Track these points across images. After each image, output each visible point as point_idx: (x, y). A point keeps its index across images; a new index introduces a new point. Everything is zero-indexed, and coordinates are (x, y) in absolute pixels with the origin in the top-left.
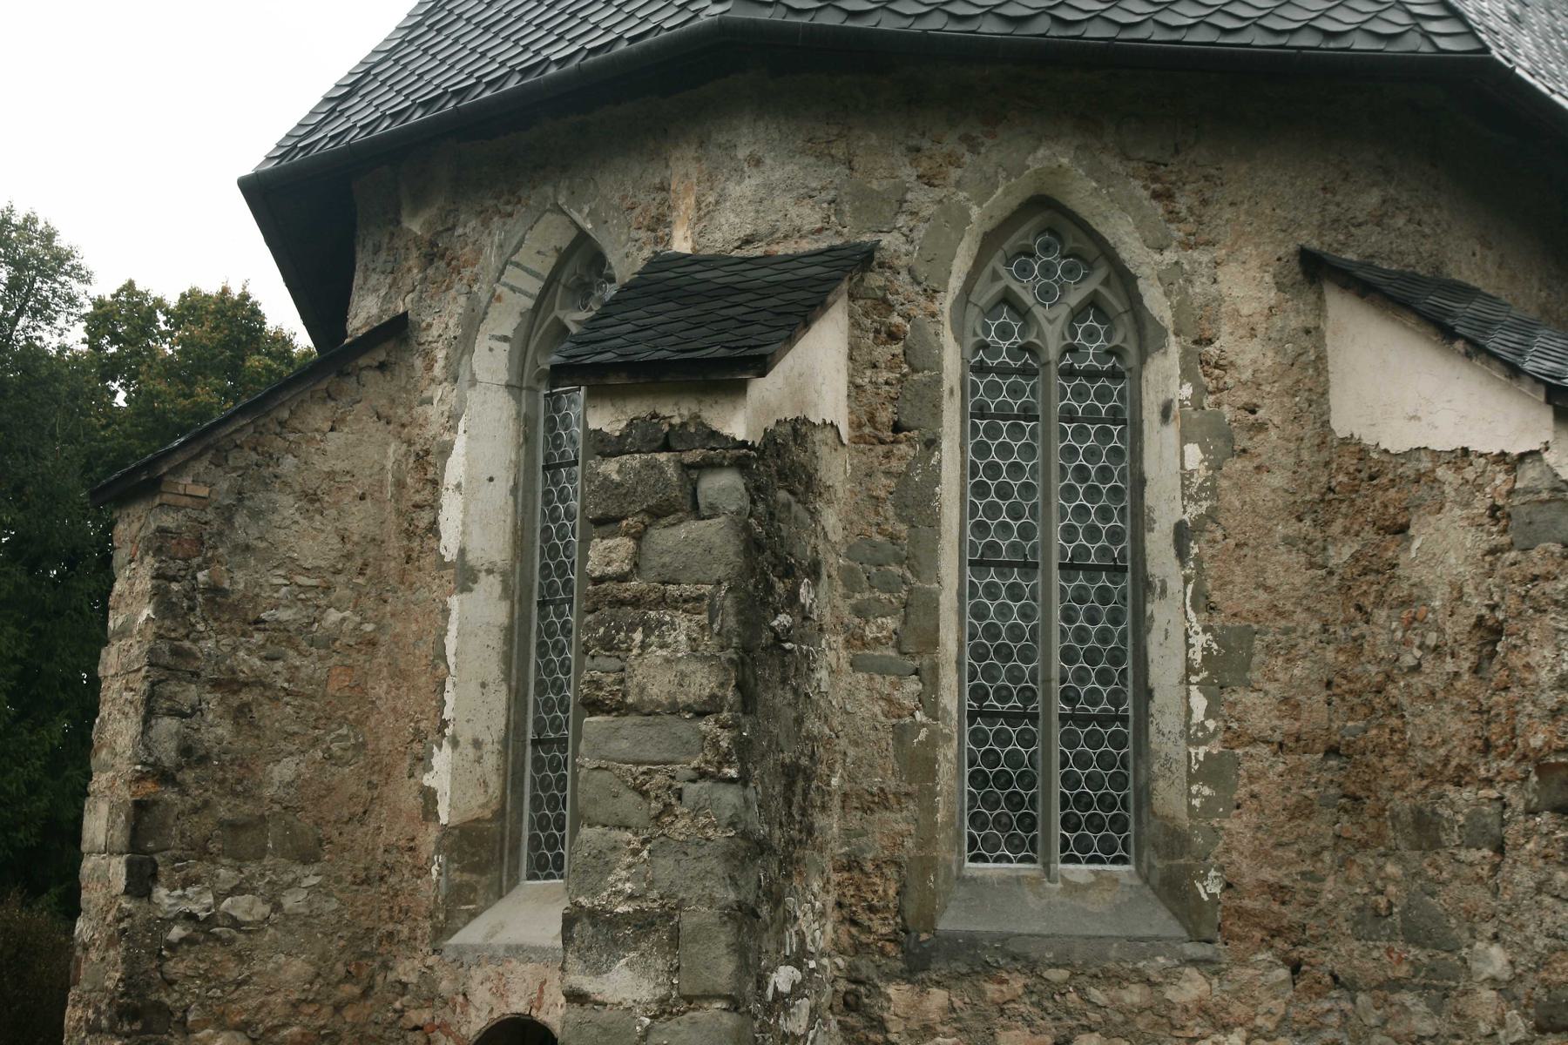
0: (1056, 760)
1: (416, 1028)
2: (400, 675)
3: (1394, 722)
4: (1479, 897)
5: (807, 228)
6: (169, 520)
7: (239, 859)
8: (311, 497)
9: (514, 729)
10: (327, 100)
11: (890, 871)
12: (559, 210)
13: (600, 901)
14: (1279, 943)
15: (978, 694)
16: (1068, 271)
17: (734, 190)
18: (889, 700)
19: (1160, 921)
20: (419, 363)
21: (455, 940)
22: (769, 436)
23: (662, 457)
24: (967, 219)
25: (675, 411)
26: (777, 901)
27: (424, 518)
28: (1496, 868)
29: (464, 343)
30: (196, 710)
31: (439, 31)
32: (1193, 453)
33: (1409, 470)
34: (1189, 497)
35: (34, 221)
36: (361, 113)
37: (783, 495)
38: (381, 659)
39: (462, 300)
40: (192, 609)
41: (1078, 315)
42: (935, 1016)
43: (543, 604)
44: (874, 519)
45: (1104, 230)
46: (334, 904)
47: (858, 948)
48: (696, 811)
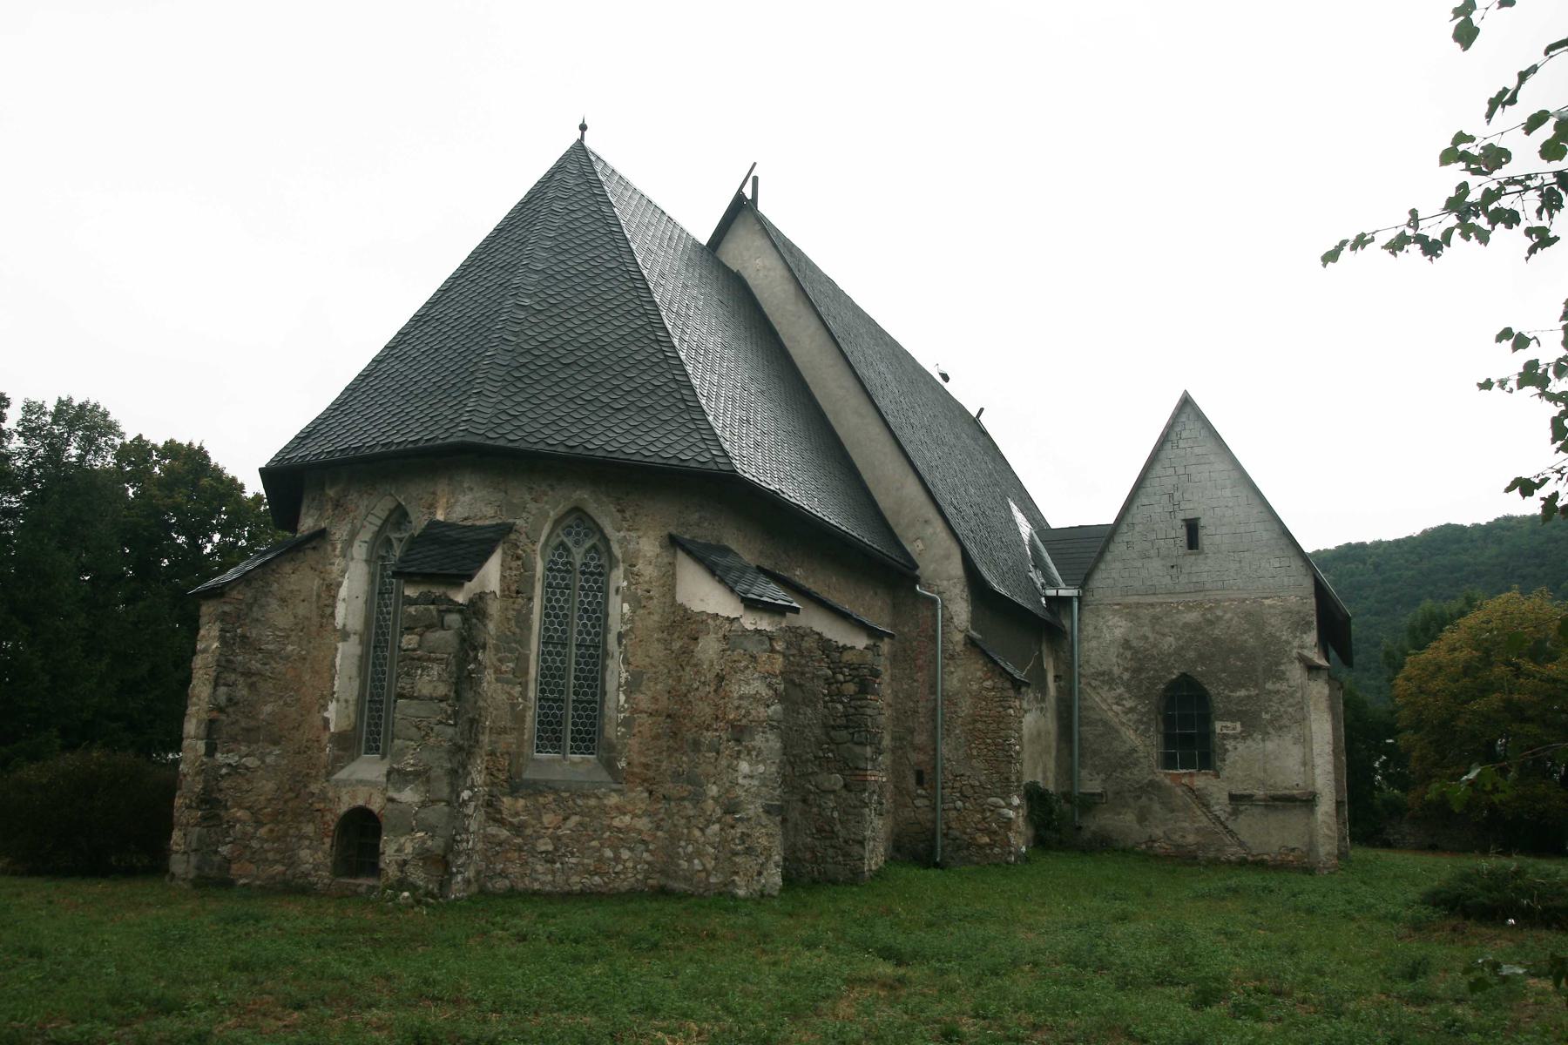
0: (570, 717)
1: (317, 810)
2: (316, 672)
3: (689, 707)
4: (711, 770)
5: (489, 515)
6: (227, 608)
7: (249, 743)
8: (283, 600)
9: (361, 695)
10: (296, 437)
11: (506, 756)
12: (391, 495)
13: (401, 766)
14: (646, 784)
15: (543, 691)
16: (586, 535)
17: (462, 499)
18: (509, 693)
19: (603, 776)
20: (329, 548)
21: (337, 776)
22: (471, 600)
23: (432, 607)
24: (548, 516)
25: (437, 591)
26: (465, 768)
27: (328, 611)
28: (716, 759)
29: (349, 543)
30: (234, 684)
31: (346, 415)
32: (626, 607)
33: (699, 618)
34: (623, 622)
35: (98, 407)
36: (312, 450)
37: (474, 621)
38: (307, 665)
39: (349, 526)
40: (234, 644)
41: (588, 551)
42: (520, 809)
43: (375, 647)
44: (506, 625)
45: (599, 521)
46: (286, 761)
47: (493, 784)
48: (438, 735)
